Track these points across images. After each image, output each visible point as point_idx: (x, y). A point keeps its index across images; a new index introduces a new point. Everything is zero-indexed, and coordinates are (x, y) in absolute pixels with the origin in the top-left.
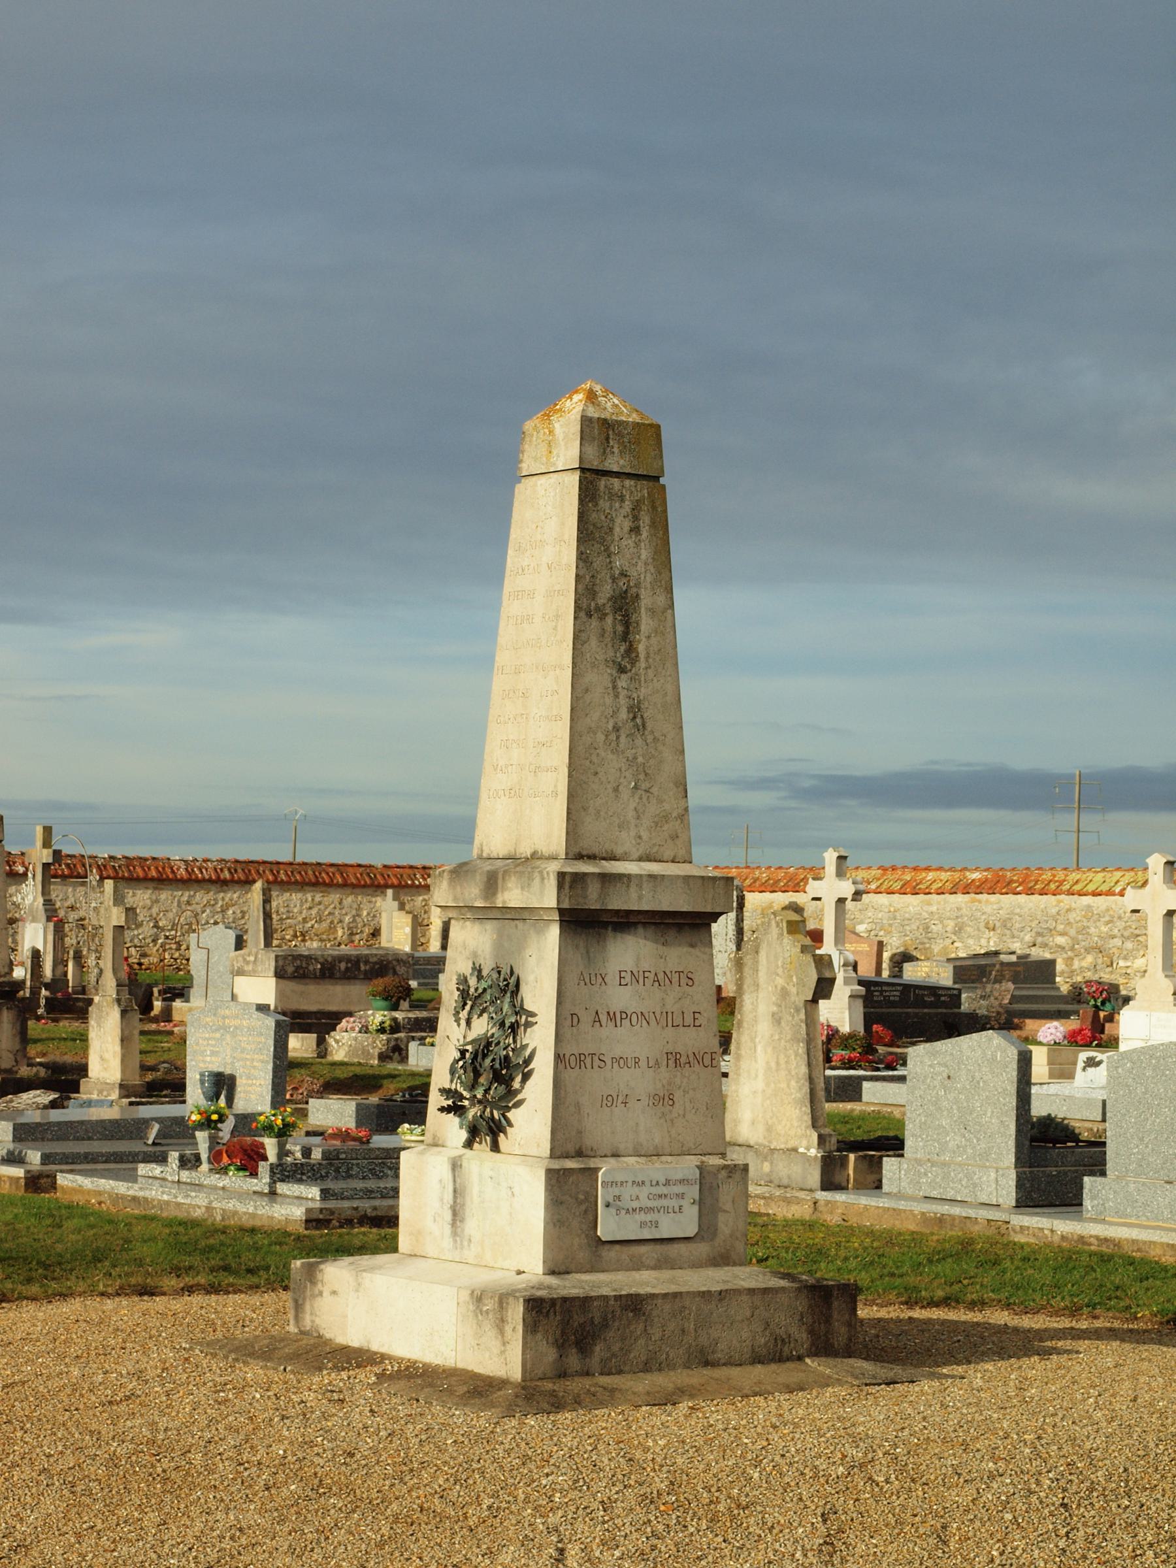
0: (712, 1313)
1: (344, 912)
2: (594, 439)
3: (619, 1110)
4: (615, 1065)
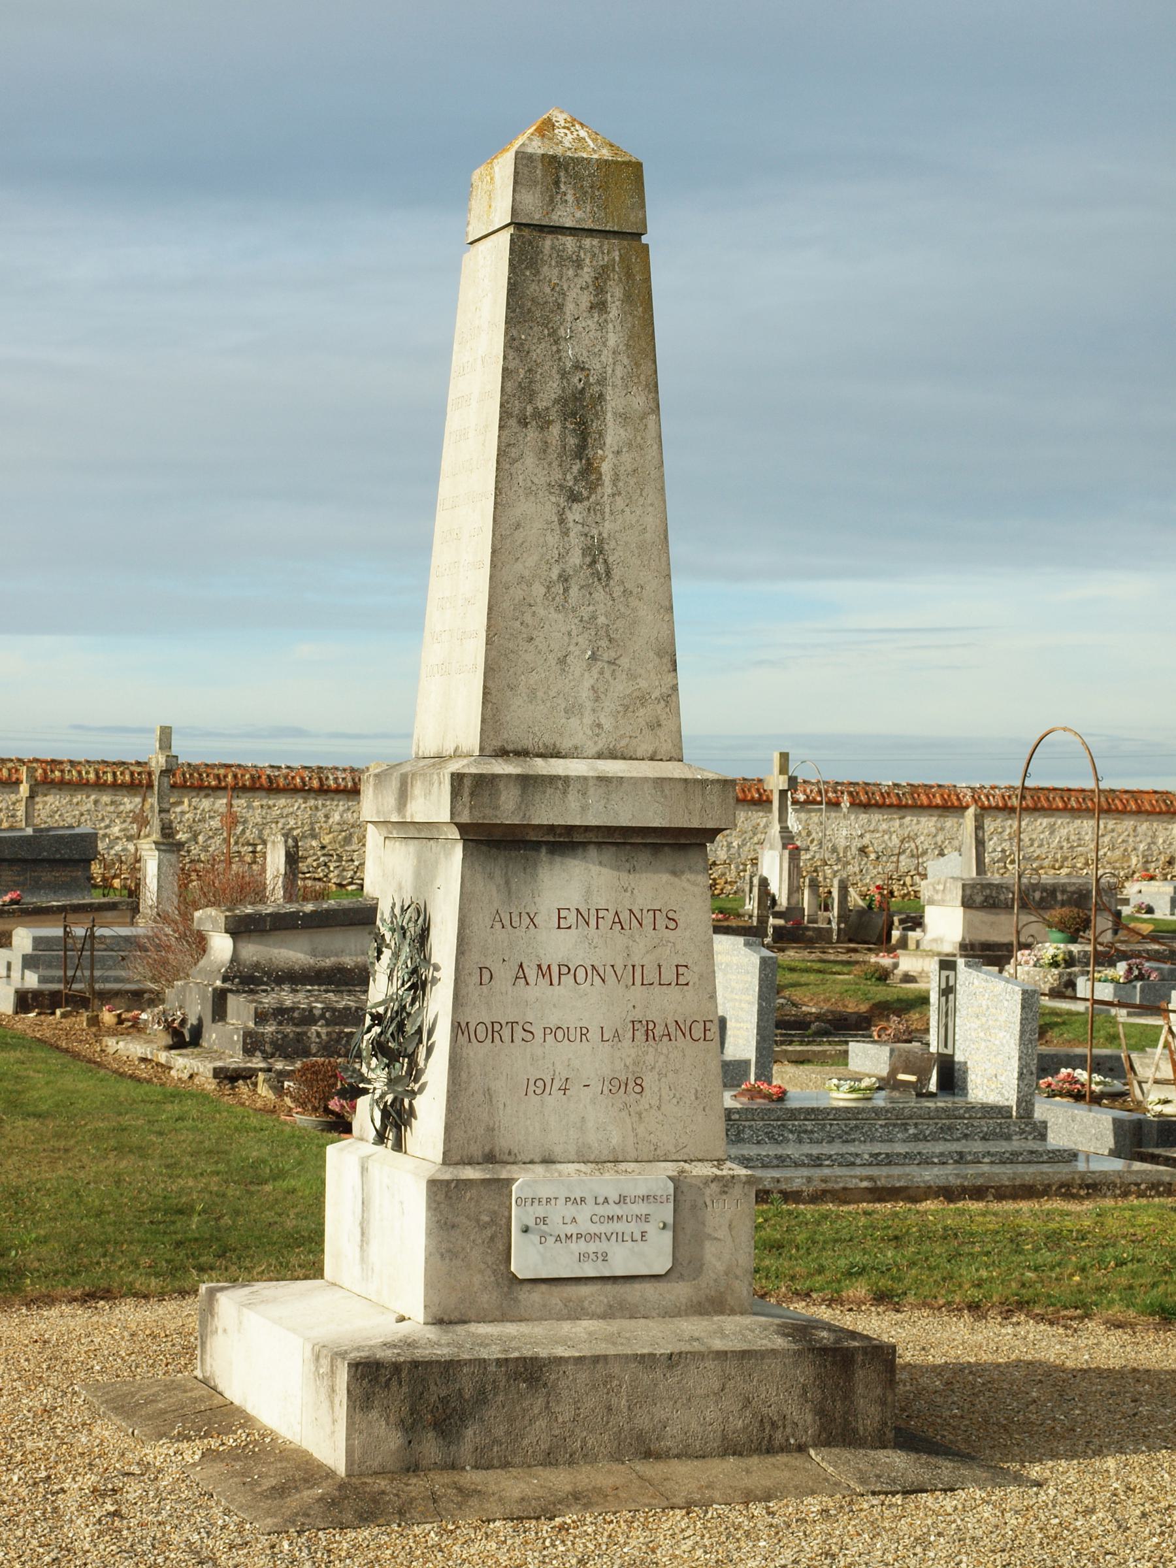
0: (656, 1385)
1: (1138, 839)
2: (536, 183)
3: (554, 1099)
4: (550, 1038)
